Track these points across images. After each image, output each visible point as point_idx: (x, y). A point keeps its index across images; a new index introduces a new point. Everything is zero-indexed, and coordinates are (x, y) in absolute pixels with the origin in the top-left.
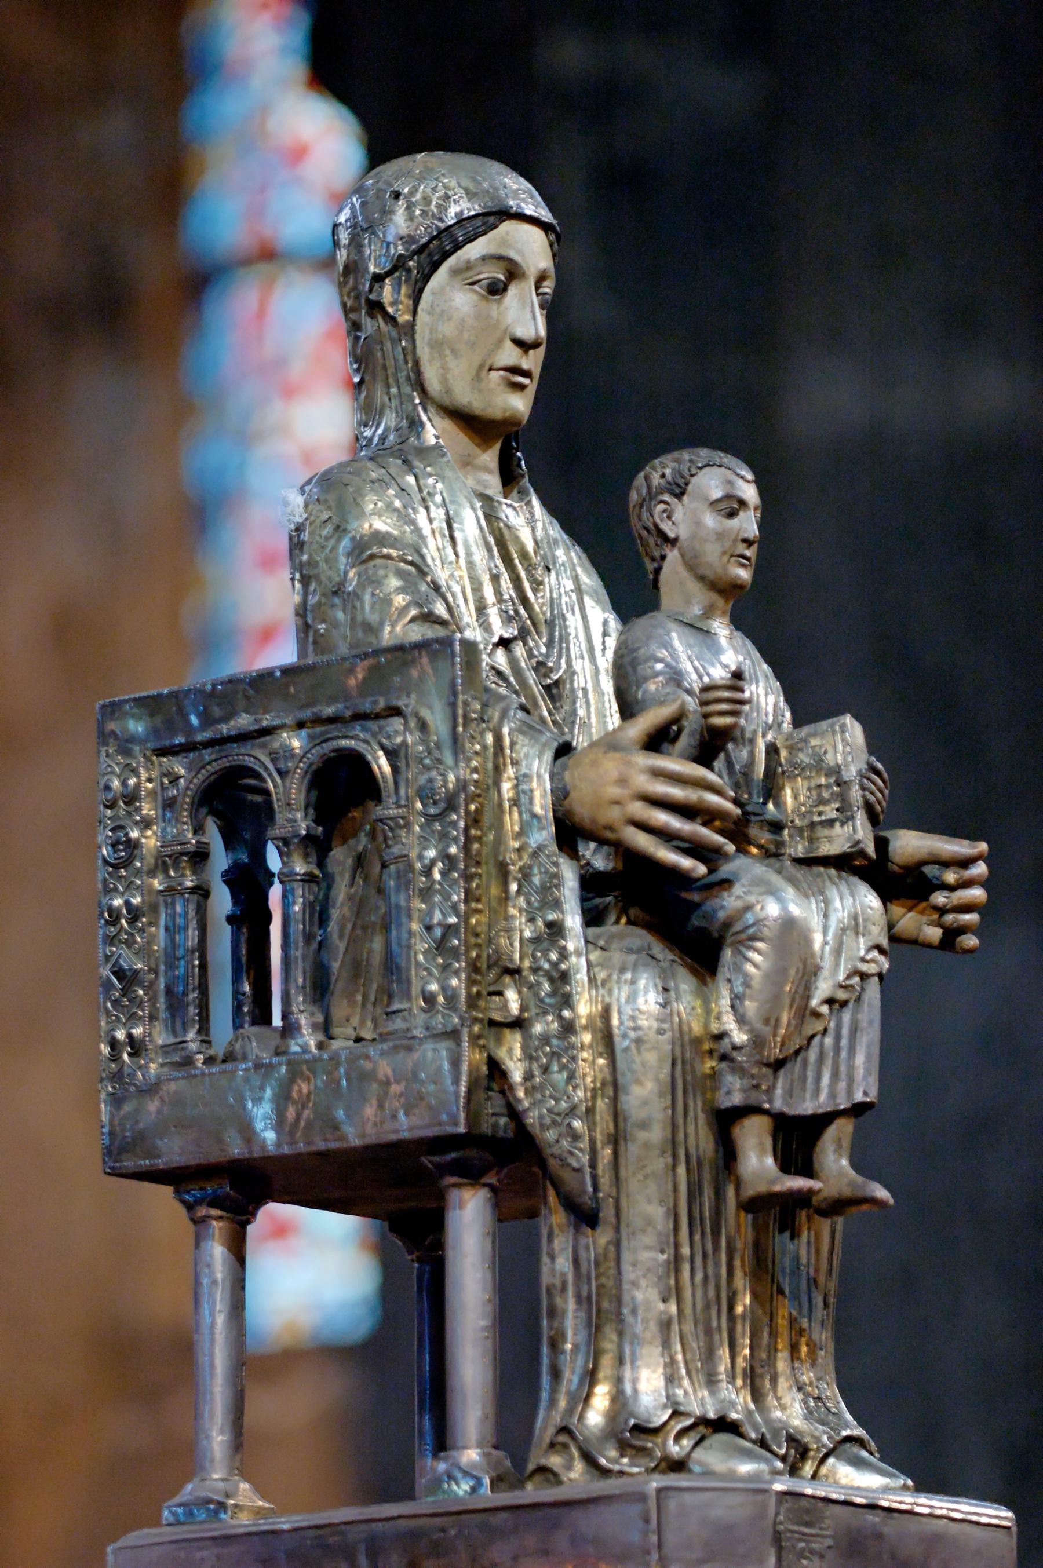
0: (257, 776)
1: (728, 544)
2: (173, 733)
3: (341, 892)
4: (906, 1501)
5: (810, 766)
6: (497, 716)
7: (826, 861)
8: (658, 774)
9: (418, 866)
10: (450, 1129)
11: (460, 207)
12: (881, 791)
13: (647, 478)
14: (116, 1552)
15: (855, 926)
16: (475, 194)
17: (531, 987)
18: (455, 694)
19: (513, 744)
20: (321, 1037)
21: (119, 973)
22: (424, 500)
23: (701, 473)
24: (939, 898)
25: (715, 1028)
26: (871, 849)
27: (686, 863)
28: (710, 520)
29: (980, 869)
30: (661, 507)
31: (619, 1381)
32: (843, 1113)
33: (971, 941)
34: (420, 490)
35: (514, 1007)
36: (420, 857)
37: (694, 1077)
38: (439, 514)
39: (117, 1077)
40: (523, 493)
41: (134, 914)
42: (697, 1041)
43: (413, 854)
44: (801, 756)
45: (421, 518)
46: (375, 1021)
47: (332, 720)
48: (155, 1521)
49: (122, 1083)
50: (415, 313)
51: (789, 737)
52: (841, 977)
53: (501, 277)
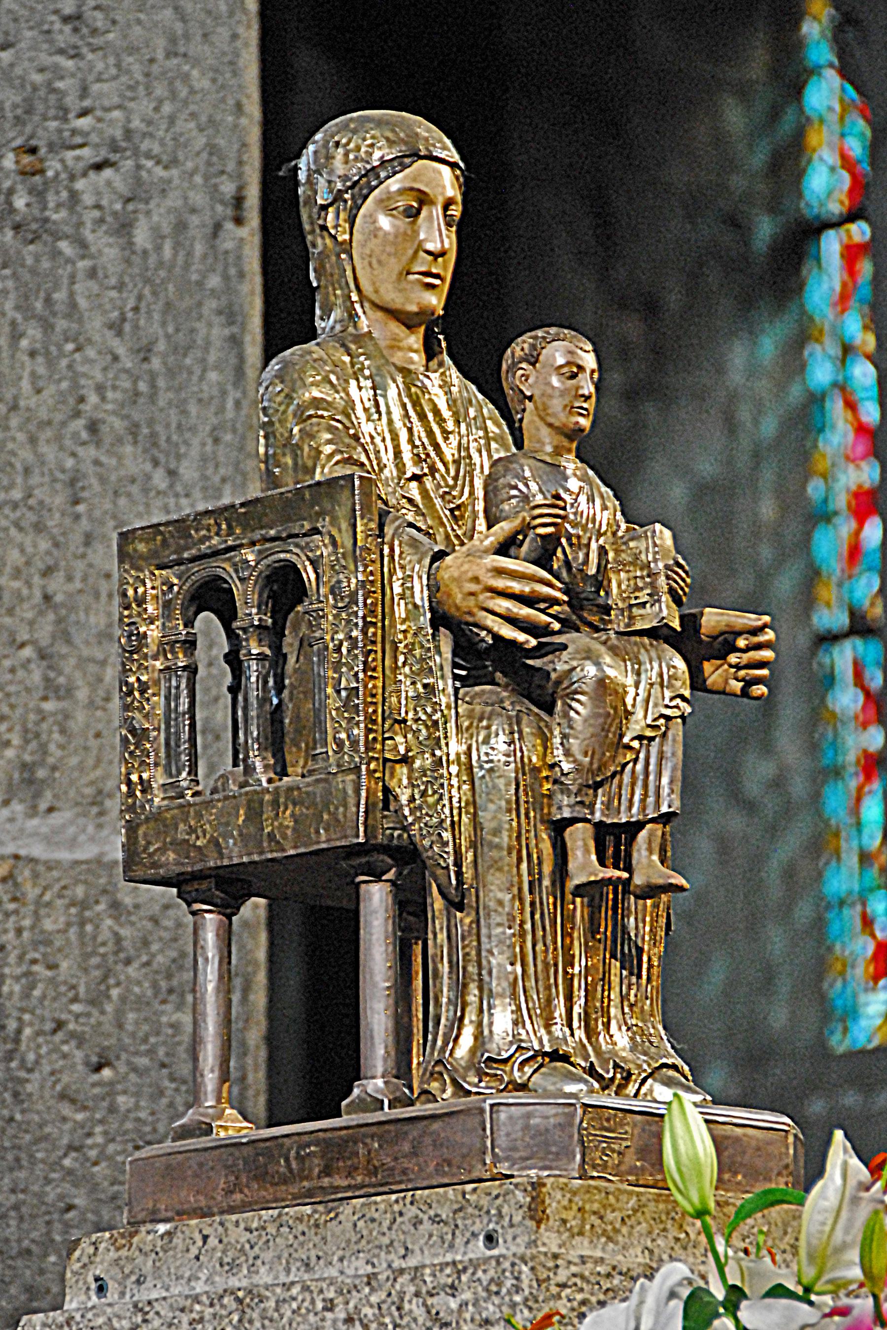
8: (500, 572)
9: (331, 645)
10: (355, 841)
12: (683, 580)
13: (513, 353)
16: (394, 142)
21: (133, 731)
24: (733, 658)
25: (550, 760)
26: (676, 624)
27: (521, 637)
30: (520, 372)
31: (480, 1024)
32: (653, 820)
33: (760, 690)
35: (402, 750)
36: (333, 639)
39: (131, 809)
42: (536, 770)
43: (328, 637)
44: (623, 555)
49: (135, 813)
50: (351, 234)
53: (415, 204)
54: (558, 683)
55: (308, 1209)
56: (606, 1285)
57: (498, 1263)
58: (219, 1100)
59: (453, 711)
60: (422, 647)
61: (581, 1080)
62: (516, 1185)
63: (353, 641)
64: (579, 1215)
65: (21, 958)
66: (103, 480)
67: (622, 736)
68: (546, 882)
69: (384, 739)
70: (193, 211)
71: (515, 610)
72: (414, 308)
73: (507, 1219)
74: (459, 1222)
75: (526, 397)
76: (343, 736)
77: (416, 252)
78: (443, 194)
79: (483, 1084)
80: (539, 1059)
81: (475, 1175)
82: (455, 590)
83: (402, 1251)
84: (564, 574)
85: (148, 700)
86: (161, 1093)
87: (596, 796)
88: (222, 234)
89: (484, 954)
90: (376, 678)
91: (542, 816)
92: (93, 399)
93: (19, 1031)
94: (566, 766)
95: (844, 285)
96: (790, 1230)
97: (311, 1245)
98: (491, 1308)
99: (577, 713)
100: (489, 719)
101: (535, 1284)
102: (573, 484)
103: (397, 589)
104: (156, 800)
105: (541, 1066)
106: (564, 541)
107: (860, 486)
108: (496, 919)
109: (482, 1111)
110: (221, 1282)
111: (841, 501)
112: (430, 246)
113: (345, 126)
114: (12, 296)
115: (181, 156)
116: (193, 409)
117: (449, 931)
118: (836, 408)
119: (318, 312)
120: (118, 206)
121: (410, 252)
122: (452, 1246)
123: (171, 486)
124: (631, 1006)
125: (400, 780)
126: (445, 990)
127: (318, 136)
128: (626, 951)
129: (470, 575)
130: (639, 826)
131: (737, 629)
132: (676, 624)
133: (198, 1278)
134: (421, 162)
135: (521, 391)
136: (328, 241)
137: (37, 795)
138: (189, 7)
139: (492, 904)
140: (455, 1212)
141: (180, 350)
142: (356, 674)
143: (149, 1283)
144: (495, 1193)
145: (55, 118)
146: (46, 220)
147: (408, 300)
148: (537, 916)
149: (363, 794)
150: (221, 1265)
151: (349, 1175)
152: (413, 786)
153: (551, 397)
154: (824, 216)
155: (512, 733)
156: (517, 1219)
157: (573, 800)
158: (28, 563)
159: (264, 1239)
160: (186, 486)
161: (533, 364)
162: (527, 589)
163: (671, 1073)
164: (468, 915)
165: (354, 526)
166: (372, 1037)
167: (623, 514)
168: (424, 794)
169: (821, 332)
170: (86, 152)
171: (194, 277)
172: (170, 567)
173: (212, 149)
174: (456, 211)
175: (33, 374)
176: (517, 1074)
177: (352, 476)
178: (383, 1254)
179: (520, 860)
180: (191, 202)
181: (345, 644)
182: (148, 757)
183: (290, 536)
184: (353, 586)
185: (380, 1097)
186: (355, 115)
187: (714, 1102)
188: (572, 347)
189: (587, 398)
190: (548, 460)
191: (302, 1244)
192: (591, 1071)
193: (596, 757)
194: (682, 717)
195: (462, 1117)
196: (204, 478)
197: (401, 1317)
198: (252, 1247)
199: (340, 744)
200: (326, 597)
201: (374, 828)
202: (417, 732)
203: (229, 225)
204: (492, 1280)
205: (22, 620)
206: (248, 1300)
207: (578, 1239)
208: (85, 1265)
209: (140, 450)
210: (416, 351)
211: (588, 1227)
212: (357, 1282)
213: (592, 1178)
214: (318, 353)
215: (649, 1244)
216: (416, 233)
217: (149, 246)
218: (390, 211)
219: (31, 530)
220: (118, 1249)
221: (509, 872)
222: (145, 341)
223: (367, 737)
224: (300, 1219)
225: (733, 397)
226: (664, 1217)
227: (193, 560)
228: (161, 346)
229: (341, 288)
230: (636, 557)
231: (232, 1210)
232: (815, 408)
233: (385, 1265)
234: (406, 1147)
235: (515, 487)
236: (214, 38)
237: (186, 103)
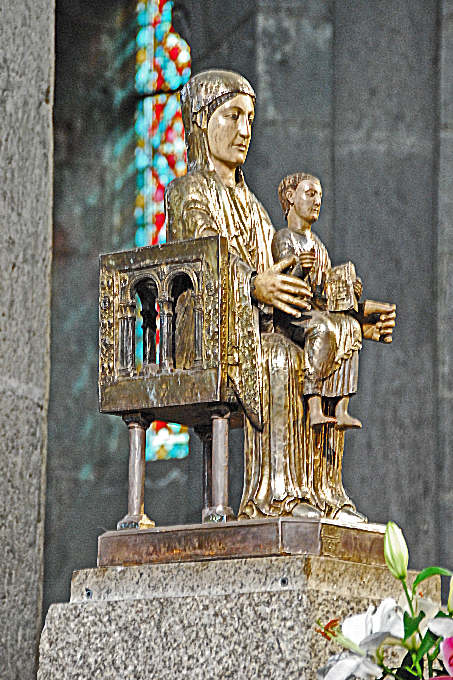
0: (151, 279)
1: (310, 206)
2: (125, 265)
3: (179, 318)
4: (363, 526)
7: (341, 312)
8: (284, 282)
10: (215, 400)
11: (223, 89)
13: (284, 183)
14: (101, 539)
15: (351, 334)
20: (172, 368)
24: (379, 324)
25: (303, 367)
26: (357, 309)
27: (294, 312)
28: (304, 197)
29: (393, 315)
31: (269, 484)
32: (346, 396)
33: (389, 339)
37: (212, 413)
38: (214, 194)
40: (242, 186)
41: (111, 326)
45: (208, 194)
46: (190, 363)
47: (177, 262)
48: (115, 528)
51: (330, 271)
54: (308, 333)
55: (193, 564)
56: (336, 604)
58: (140, 512)
62: (298, 559)
67: (334, 358)
70: (31, 96)
72: (234, 160)
73: (293, 574)
74: (269, 574)
76: (210, 352)
77: (236, 136)
86: (8, 493)
87: (323, 385)
88: (41, 108)
94: (311, 370)
95: (154, 123)
98: (287, 613)
101: (309, 604)
103: (236, 288)
104: (116, 377)
105: (297, 505)
107: (158, 212)
108: (278, 437)
109: (277, 524)
110: (150, 595)
111: (149, 219)
113: (205, 77)
115: (27, 71)
116: (28, 185)
118: (148, 175)
121: (234, 135)
122: (265, 584)
123: (19, 220)
124: (331, 478)
129: (271, 283)
130: (340, 398)
132: (357, 309)
133: (137, 592)
136: (196, 128)
138: (31, 3)
139: (276, 431)
140: (267, 569)
141: (24, 159)
143: (113, 592)
144: (286, 561)
147: (232, 156)
150: (149, 587)
154: (145, 91)
156: (298, 573)
159: (171, 576)
160: (25, 220)
168: (247, 380)
169: (143, 142)
178: (230, 586)
181: (212, 312)
183: (186, 261)
191: (190, 580)
193: (325, 367)
195: (267, 527)
196: (32, 217)
197: (242, 615)
198: (165, 580)
199: (209, 356)
201: (224, 395)
203: (44, 103)
204: (287, 601)
206: (165, 604)
208: (81, 584)
209: (7, 203)
212: (220, 598)
216: (236, 126)
217: (13, 112)
220: (97, 577)
222: (10, 155)
224: (189, 568)
225: (104, 169)
227: (137, 269)
228: (16, 157)
230: (340, 278)
232: (139, 176)
234: (239, 538)
236: (41, 19)
237: (29, 47)
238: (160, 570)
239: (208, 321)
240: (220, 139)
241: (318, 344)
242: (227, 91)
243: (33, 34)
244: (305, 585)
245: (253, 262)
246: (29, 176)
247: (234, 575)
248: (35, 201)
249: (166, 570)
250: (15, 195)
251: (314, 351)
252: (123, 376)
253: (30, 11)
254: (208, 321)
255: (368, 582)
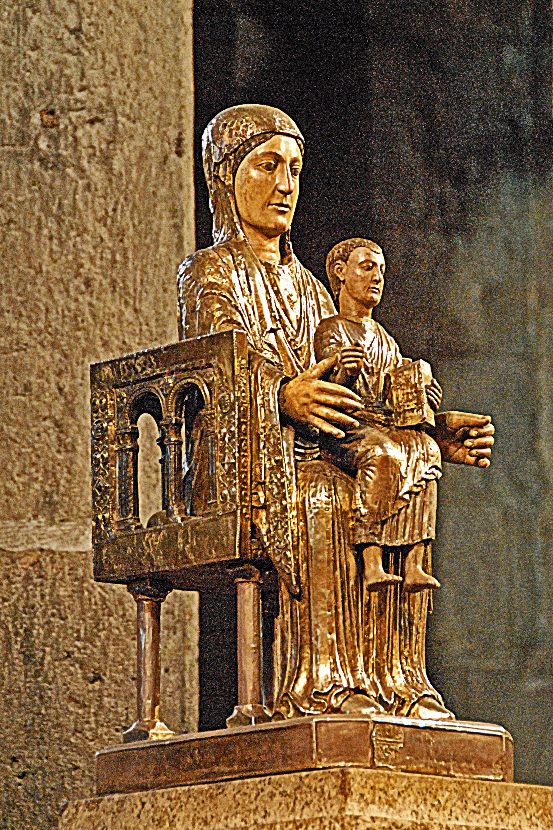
5: (404, 384)
6: (256, 366)
7: (411, 428)
8: (322, 391)
10: (233, 557)
11: (253, 130)
13: (333, 254)
17: (269, 490)
18: (233, 357)
19: (262, 379)
21: (99, 489)
22: (235, 266)
23: (355, 250)
24: (468, 443)
25: (354, 507)
26: (433, 423)
27: (335, 431)
30: (337, 266)
31: (311, 671)
34: (234, 262)
35: (262, 500)
36: (220, 432)
38: (242, 273)
42: (345, 513)
44: (400, 379)
47: (184, 370)
52: (416, 481)
53: (273, 162)
54: (359, 459)
55: (206, 787)
57: (321, 822)
59: (294, 477)
60: (274, 437)
61: (372, 705)
63: (232, 433)
64: (371, 792)
65: (44, 613)
66: (94, 316)
67: (398, 492)
68: (352, 583)
69: (252, 494)
70: (150, 148)
71: (332, 414)
72: (272, 226)
73: (327, 794)
74: (298, 796)
75: (340, 281)
78: (290, 155)
79: (312, 708)
80: (348, 693)
81: (307, 765)
82: (295, 402)
83: (263, 814)
84: (363, 391)
85: (108, 469)
87: (382, 529)
89: (313, 627)
90: (246, 456)
91: (349, 541)
92: (87, 265)
93: (43, 658)
96: (503, 798)
97: (208, 809)
99: (371, 478)
100: (316, 481)
102: (369, 335)
103: (259, 401)
105: (348, 697)
106: (363, 370)
109: (310, 726)
112: (282, 188)
114: (39, 203)
117: (292, 613)
119: (214, 228)
120: (104, 146)
121: (270, 192)
122: (293, 810)
124: (406, 658)
125: (261, 519)
126: (289, 649)
127: (214, 121)
128: (402, 624)
129: (304, 392)
130: (409, 547)
131: (471, 424)
132: (433, 423)
134: (277, 136)
135: (338, 278)
136: (220, 185)
137: (55, 511)
140: (295, 790)
142: (234, 454)
145: (66, 92)
146: (59, 155)
148: (346, 604)
149: (238, 528)
150: (153, 821)
151: (231, 765)
152: (269, 523)
153: (356, 282)
155: (330, 490)
156: (333, 794)
157: (368, 531)
158: (48, 368)
159: (179, 805)
161: (345, 261)
162: (339, 401)
163: (430, 700)
164: (304, 603)
165: (233, 363)
166: (245, 679)
167: (401, 352)
168: (276, 528)
170: (84, 113)
171: (151, 189)
172: (122, 387)
173: (162, 109)
174: (299, 166)
175: (51, 250)
176: (333, 701)
177: (232, 332)
178: (252, 815)
179: (335, 569)
180: (149, 143)
181: (227, 435)
182: (108, 504)
183: (194, 368)
184: (232, 399)
185: (249, 715)
186: (236, 107)
187: (457, 718)
188: (368, 251)
189: (378, 282)
190: (354, 319)
191: (202, 809)
192: (380, 699)
194: (436, 479)
198: (172, 810)
199: (224, 497)
200: (216, 406)
201: (245, 549)
202: (271, 490)
205: (45, 403)
207: (371, 806)
210: (274, 252)
211: (377, 799)
213: (379, 767)
214: (214, 255)
215: (415, 808)
216: (274, 179)
218: (257, 167)
219: (49, 347)
220: (90, 810)
221: (328, 576)
223: (241, 493)
224: (201, 792)
226: (424, 791)
228: (131, 232)
229: (227, 213)
230: (408, 381)
231: (159, 786)
233: (252, 822)
235: (333, 337)
238: (166, 796)
239: (222, 450)
240: (250, 197)
241: (372, 475)
242: (258, 131)
243: (152, 63)
244: (342, 810)
245: (301, 364)
246: (151, 258)
247: (256, 799)
248: (161, 290)
249: (173, 796)
250: (130, 284)
251: (366, 484)
252: (121, 530)
253: (145, 31)
254: (222, 450)
255: (447, 801)
